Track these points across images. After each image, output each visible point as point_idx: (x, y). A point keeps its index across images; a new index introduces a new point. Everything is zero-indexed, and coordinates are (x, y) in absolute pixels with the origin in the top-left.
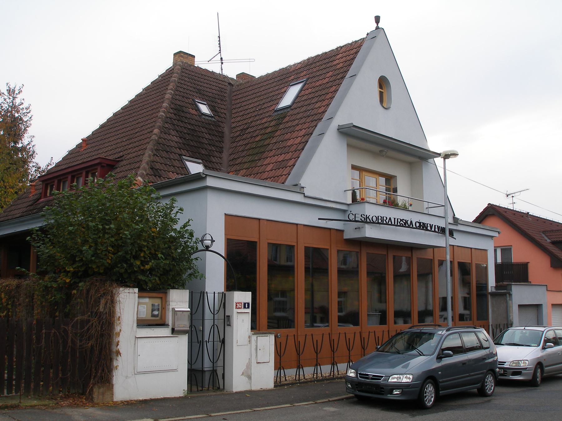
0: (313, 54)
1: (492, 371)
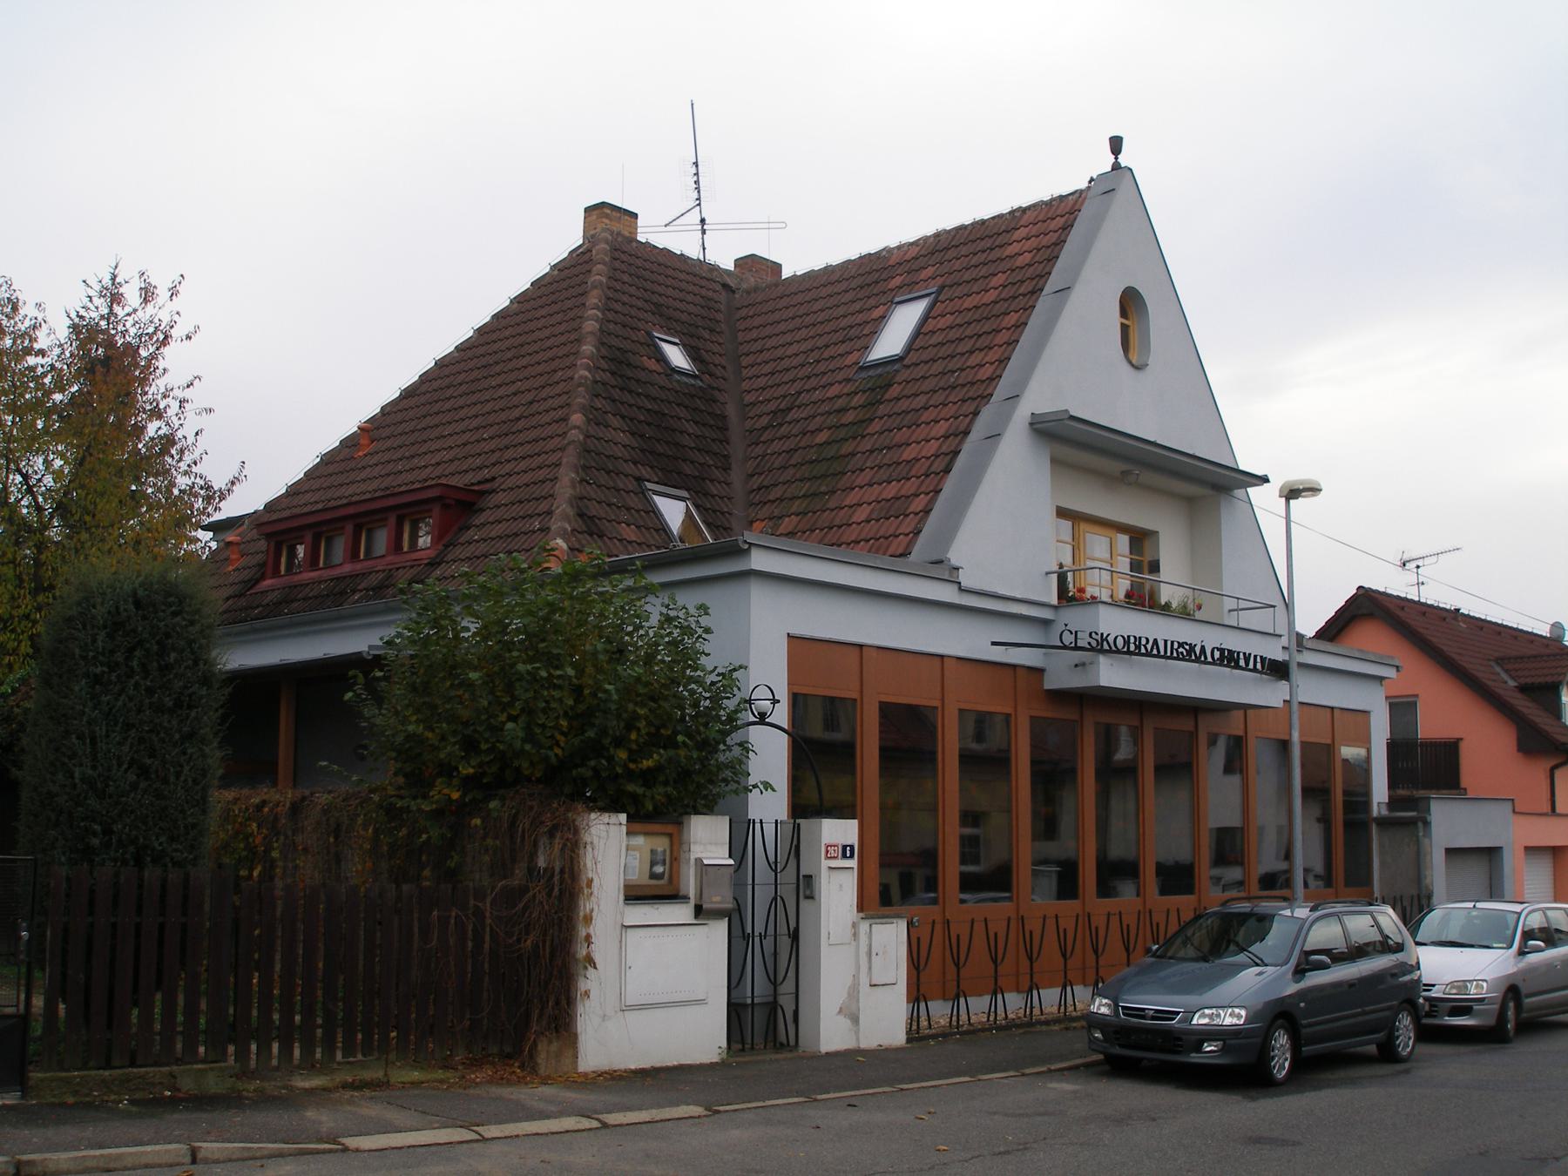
0: (950, 223)
1: (1410, 1004)
